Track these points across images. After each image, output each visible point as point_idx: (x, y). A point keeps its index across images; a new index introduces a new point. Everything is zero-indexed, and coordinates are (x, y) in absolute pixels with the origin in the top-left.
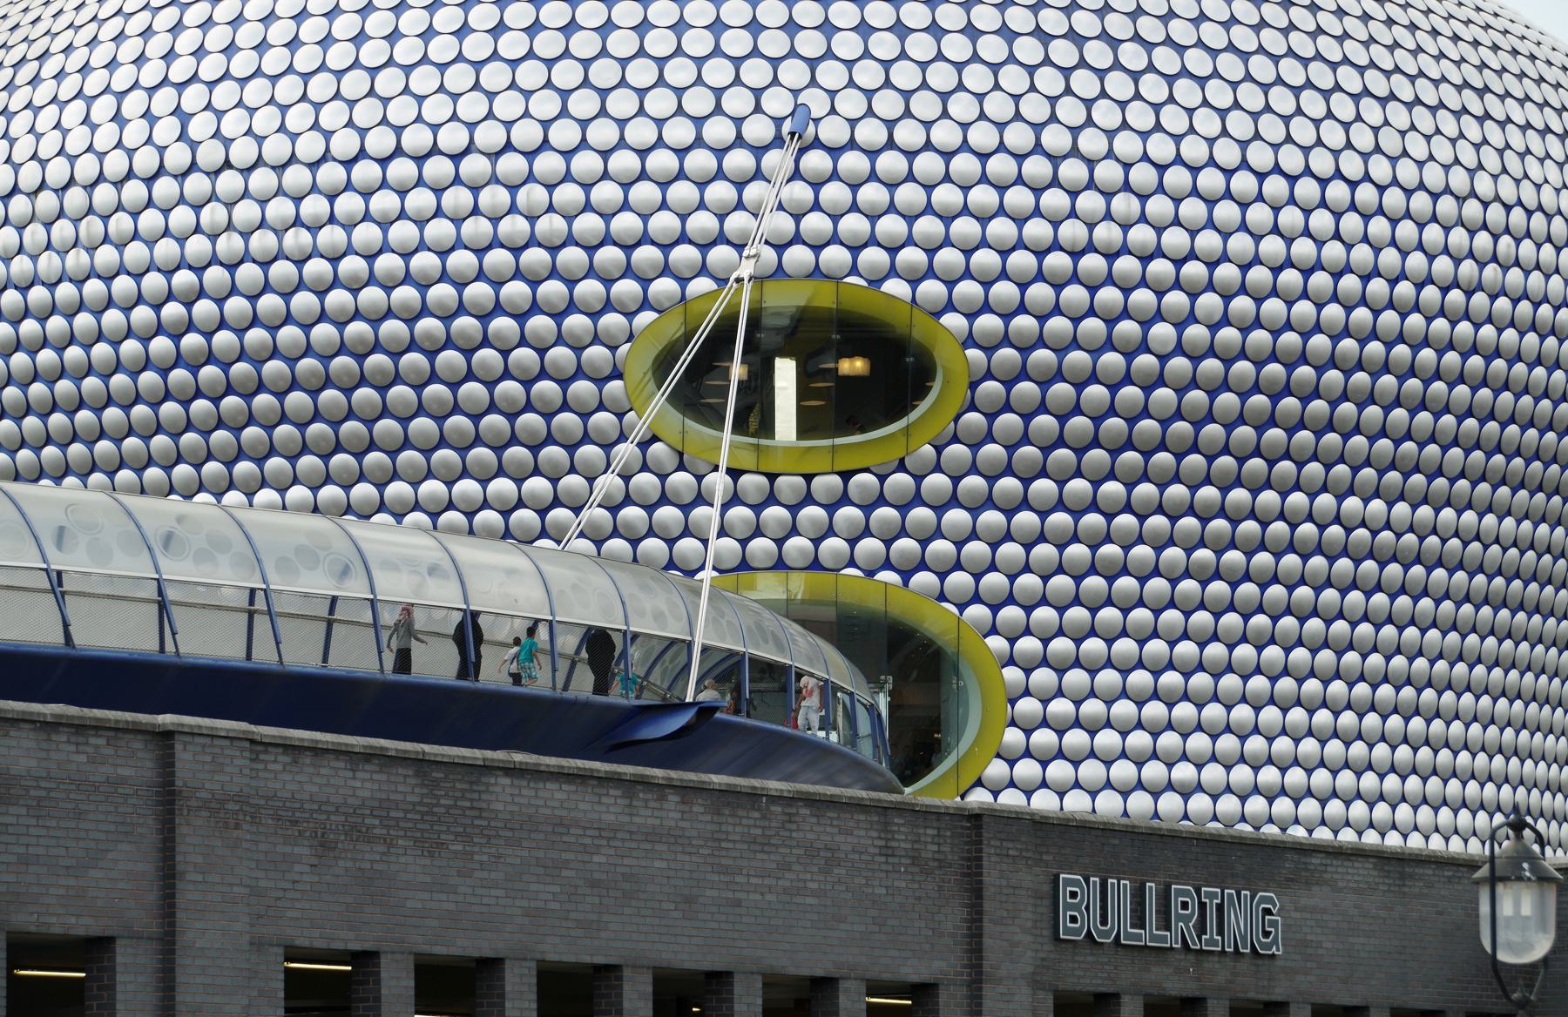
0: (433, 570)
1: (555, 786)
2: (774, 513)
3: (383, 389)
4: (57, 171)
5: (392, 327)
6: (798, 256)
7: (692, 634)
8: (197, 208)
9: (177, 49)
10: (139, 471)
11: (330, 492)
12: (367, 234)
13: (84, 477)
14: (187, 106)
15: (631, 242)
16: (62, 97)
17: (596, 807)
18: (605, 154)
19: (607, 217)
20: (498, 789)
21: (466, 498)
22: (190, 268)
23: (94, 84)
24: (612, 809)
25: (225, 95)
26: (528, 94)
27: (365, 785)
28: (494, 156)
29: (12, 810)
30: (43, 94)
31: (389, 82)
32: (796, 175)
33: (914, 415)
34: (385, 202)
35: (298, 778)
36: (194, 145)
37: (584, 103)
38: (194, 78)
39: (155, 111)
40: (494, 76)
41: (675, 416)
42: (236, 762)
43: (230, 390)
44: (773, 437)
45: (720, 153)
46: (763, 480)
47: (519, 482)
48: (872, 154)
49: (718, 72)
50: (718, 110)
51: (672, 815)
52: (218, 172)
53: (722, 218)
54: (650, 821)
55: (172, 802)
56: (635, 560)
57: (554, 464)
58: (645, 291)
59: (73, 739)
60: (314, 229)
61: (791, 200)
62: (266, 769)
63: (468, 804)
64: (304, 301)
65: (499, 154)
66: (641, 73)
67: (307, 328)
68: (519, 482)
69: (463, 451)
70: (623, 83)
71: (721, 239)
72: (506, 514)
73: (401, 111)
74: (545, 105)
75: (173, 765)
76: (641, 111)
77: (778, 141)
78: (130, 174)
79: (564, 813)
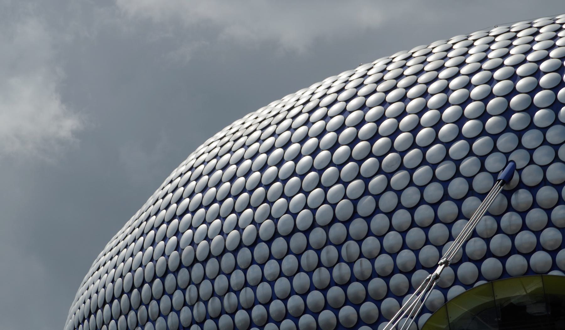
6: (516, 262)
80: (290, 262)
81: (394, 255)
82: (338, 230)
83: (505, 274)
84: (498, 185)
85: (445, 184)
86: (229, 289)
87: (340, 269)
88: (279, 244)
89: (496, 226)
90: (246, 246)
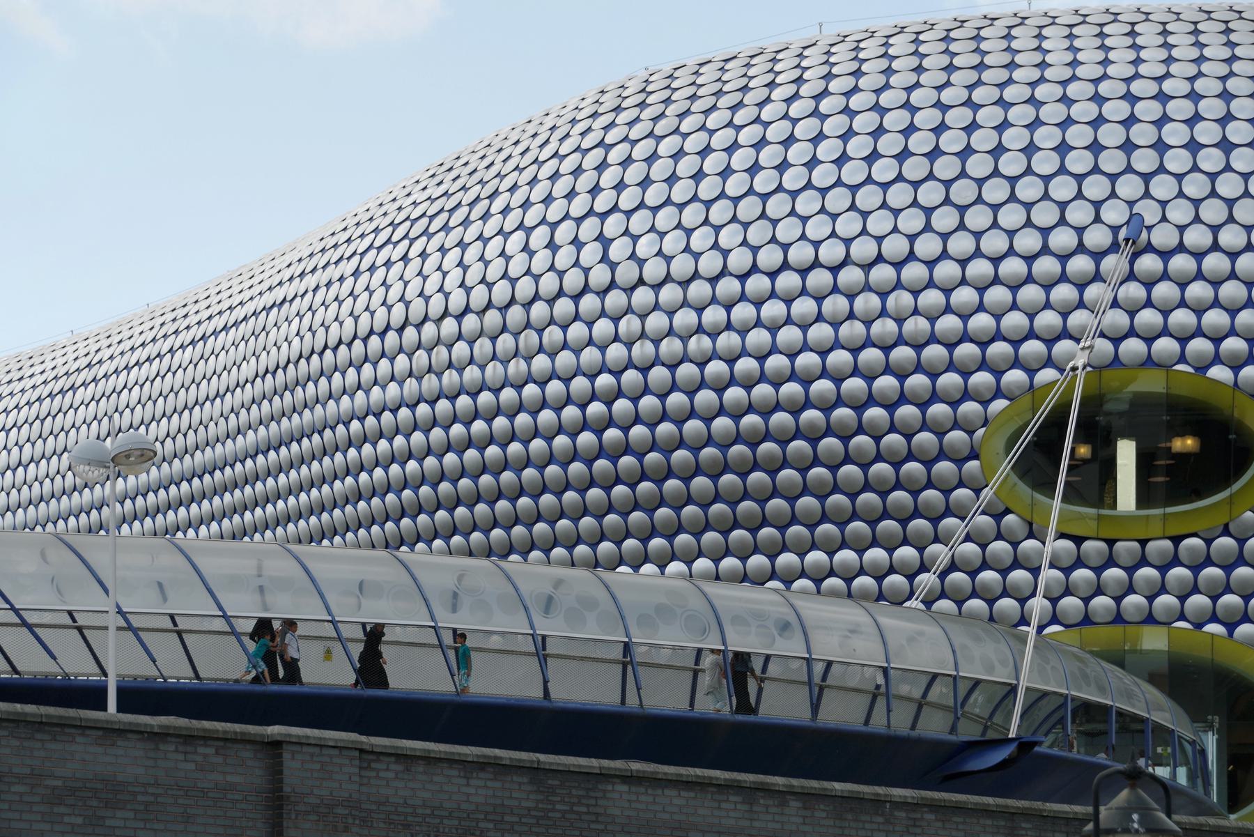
0: (785, 627)
1: (673, 793)
2: (1114, 574)
3: (773, 473)
4: (501, 291)
5: (780, 418)
6: (1133, 347)
7: (1018, 679)
8: (616, 320)
9: (602, 184)
10: (570, 548)
11: (729, 563)
12: (758, 337)
13: (525, 554)
14: (608, 232)
15: (986, 340)
16: (507, 229)
17: (716, 813)
18: (963, 263)
19: (965, 318)
20: (616, 796)
21: (844, 564)
22: (610, 372)
23: (532, 217)
24: (732, 814)
25: (639, 222)
26: (896, 212)
27: (480, 791)
28: (867, 267)
29: (119, 814)
30: (491, 227)
31: (777, 206)
32: (1131, 276)
33: (1236, 486)
34: (774, 309)
35: (411, 785)
36: (613, 266)
37: (945, 219)
38: (615, 208)
39: (582, 238)
40: (868, 198)
41: (1024, 489)
42: (345, 770)
43: (643, 477)
44: (1114, 505)
45: (1064, 258)
47: (890, 551)
48: (1199, 256)
49: (1062, 189)
50: (1062, 221)
51: (793, 819)
52: (633, 288)
53: (1065, 315)
54: (771, 825)
55: (281, 807)
56: (991, 619)
57: (920, 533)
58: (998, 381)
59: (181, 748)
60: (714, 336)
61: (1127, 299)
62: (377, 777)
63: (584, 809)
64: (705, 397)
65: (871, 265)
66: (995, 192)
67: (708, 421)
68: (890, 551)
69: (842, 525)
70: (979, 200)
71: (1065, 334)
72: (879, 579)
73: (789, 230)
74: (912, 221)
75: (281, 772)
76: (995, 225)
77: (1114, 247)
78: (560, 293)
79: (683, 818)
87: (699, 341)
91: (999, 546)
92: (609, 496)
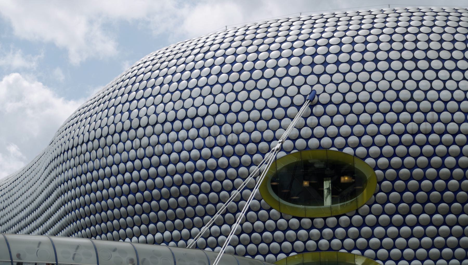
2: (314, 231)
37: (243, 95)
44: (323, 205)
46: (322, 220)
66: (262, 83)
80: (193, 132)
81: (250, 133)
82: (220, 118)
83: (307, 147)
84: (307, 102)
85: (279, 99)
86: (158, 143)
87: (221, 137)
88: (188, 122)
89: (304, 122)
90: (169, 121)
91: (270, 222)
92: (384, 174)
